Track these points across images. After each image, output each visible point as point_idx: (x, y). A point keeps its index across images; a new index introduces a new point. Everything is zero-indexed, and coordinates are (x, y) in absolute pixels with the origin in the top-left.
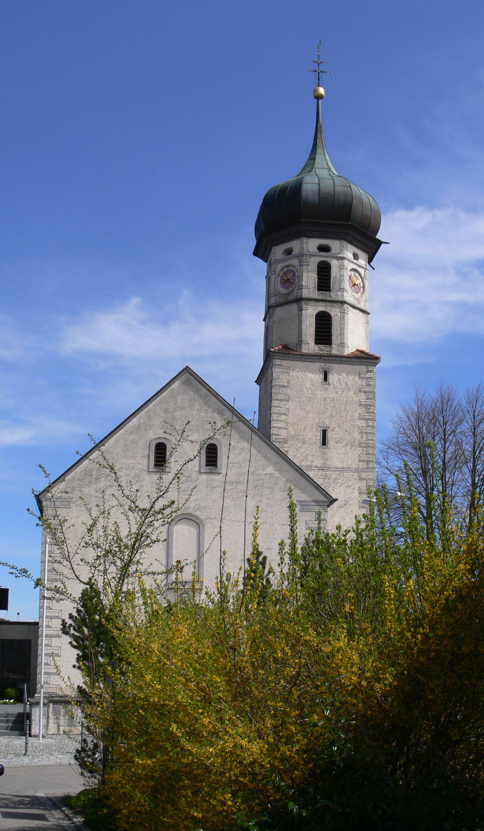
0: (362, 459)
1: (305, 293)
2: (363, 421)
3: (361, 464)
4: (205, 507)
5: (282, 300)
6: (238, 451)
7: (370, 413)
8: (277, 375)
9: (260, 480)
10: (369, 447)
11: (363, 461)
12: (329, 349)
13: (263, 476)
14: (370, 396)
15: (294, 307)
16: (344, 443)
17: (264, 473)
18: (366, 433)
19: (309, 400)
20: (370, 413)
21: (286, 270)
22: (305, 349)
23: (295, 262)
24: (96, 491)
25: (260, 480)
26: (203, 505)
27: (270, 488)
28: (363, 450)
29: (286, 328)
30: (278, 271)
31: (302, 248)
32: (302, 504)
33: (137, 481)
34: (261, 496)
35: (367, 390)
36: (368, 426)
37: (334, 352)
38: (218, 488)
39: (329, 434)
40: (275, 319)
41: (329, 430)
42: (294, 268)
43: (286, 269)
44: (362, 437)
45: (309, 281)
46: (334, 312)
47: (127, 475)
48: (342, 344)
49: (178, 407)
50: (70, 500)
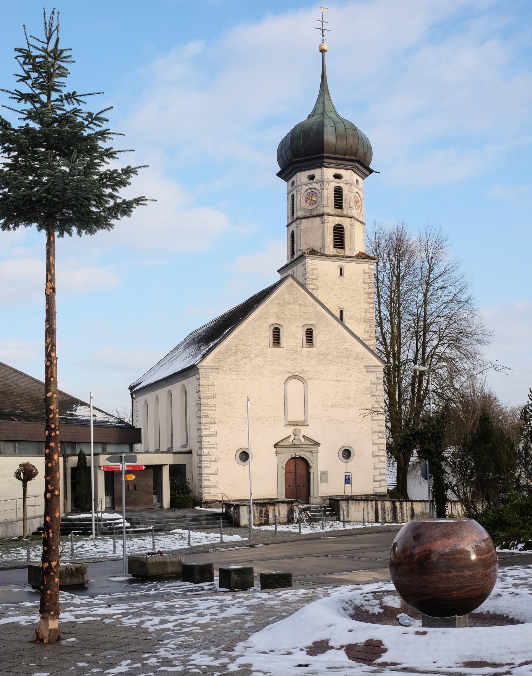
0: (367, 331)
1: (326, 210)
2: (366, 304)
3: (366, 334)
4: (306, 371)
5: (308, 214)
6: (326, 333)
7: (371, 298)
8: (309, 271)
9: (341, 352)
10: (371, 322)
11: (368, 332)
12: (343, 252)
13: (342, 350)
14: (371, 286)
15: (318, 220)
16: (355, 319)
17: (343, 347)
18: (369, 313)
19: (331, 289)
20: (371, 298)
21: (309, 191)
22: (327, 252)
23: (317, 186)
24: (235, 361)
25: (341, 352)
26: (305, 370)
27: (347, 357)
28: (367, 325)
29: (312, 235)
30: (303, 191)
31: (323, 176)
32: (368, 368)
33: (262, 354)
34: (342, 363)
35: (368, 281)
36: (370, 308)
37: (346, 254)
38: (314, 358)
39: (345, 313)
40: (302, 228)
41: (345, 310)
42: (316, 190)
43: (309, 191)
44: (366, 315)
45: (328, 201)
46: (346, 223)
47: (255, 350)
48: (352, 249)
49: (286, 302)
50: (218, 368)
